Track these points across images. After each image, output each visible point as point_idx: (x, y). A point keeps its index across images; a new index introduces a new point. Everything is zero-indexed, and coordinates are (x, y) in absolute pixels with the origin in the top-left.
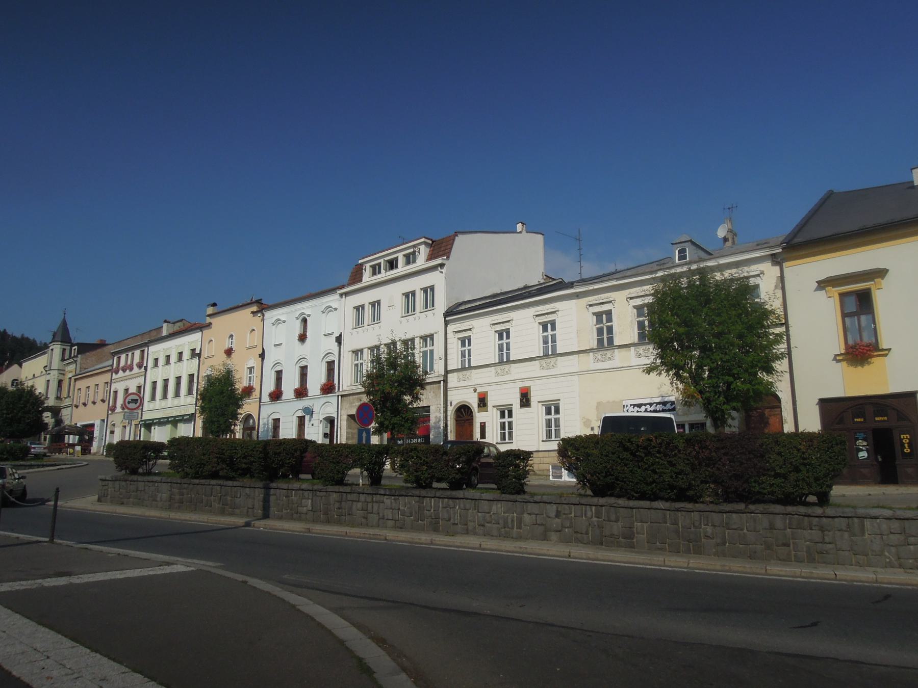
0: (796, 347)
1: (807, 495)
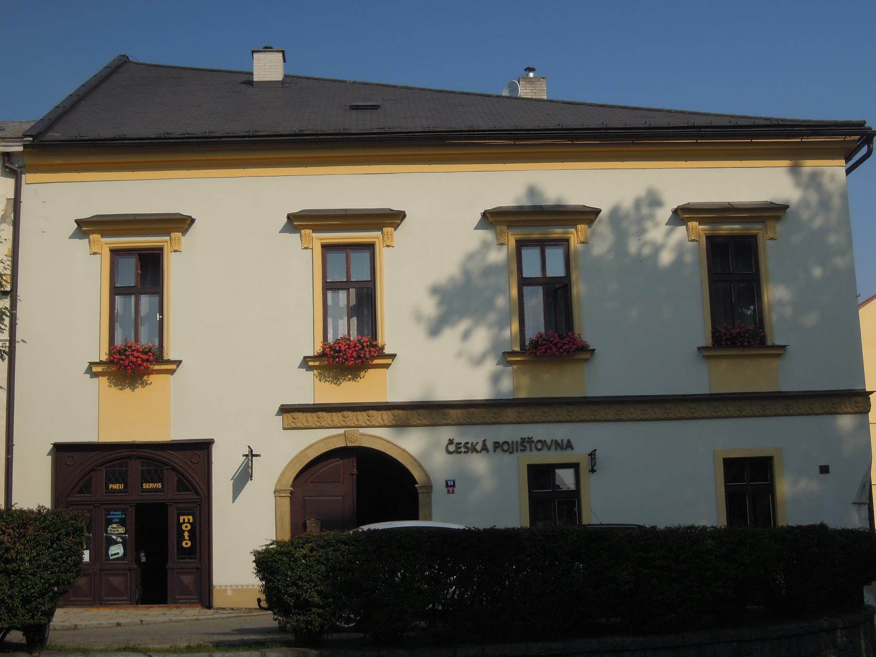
0: (23, 341)
1: (8, 630)
